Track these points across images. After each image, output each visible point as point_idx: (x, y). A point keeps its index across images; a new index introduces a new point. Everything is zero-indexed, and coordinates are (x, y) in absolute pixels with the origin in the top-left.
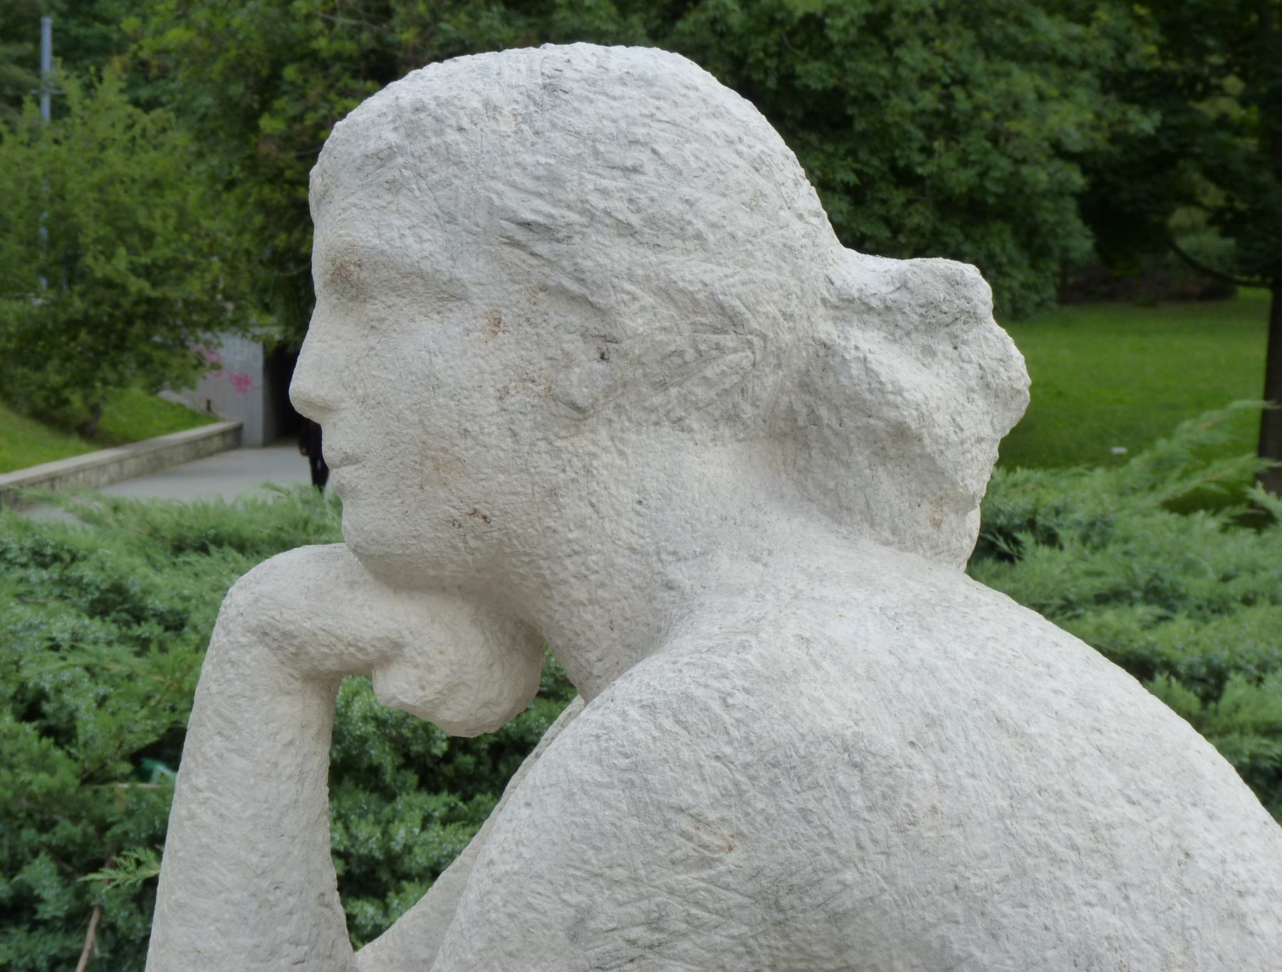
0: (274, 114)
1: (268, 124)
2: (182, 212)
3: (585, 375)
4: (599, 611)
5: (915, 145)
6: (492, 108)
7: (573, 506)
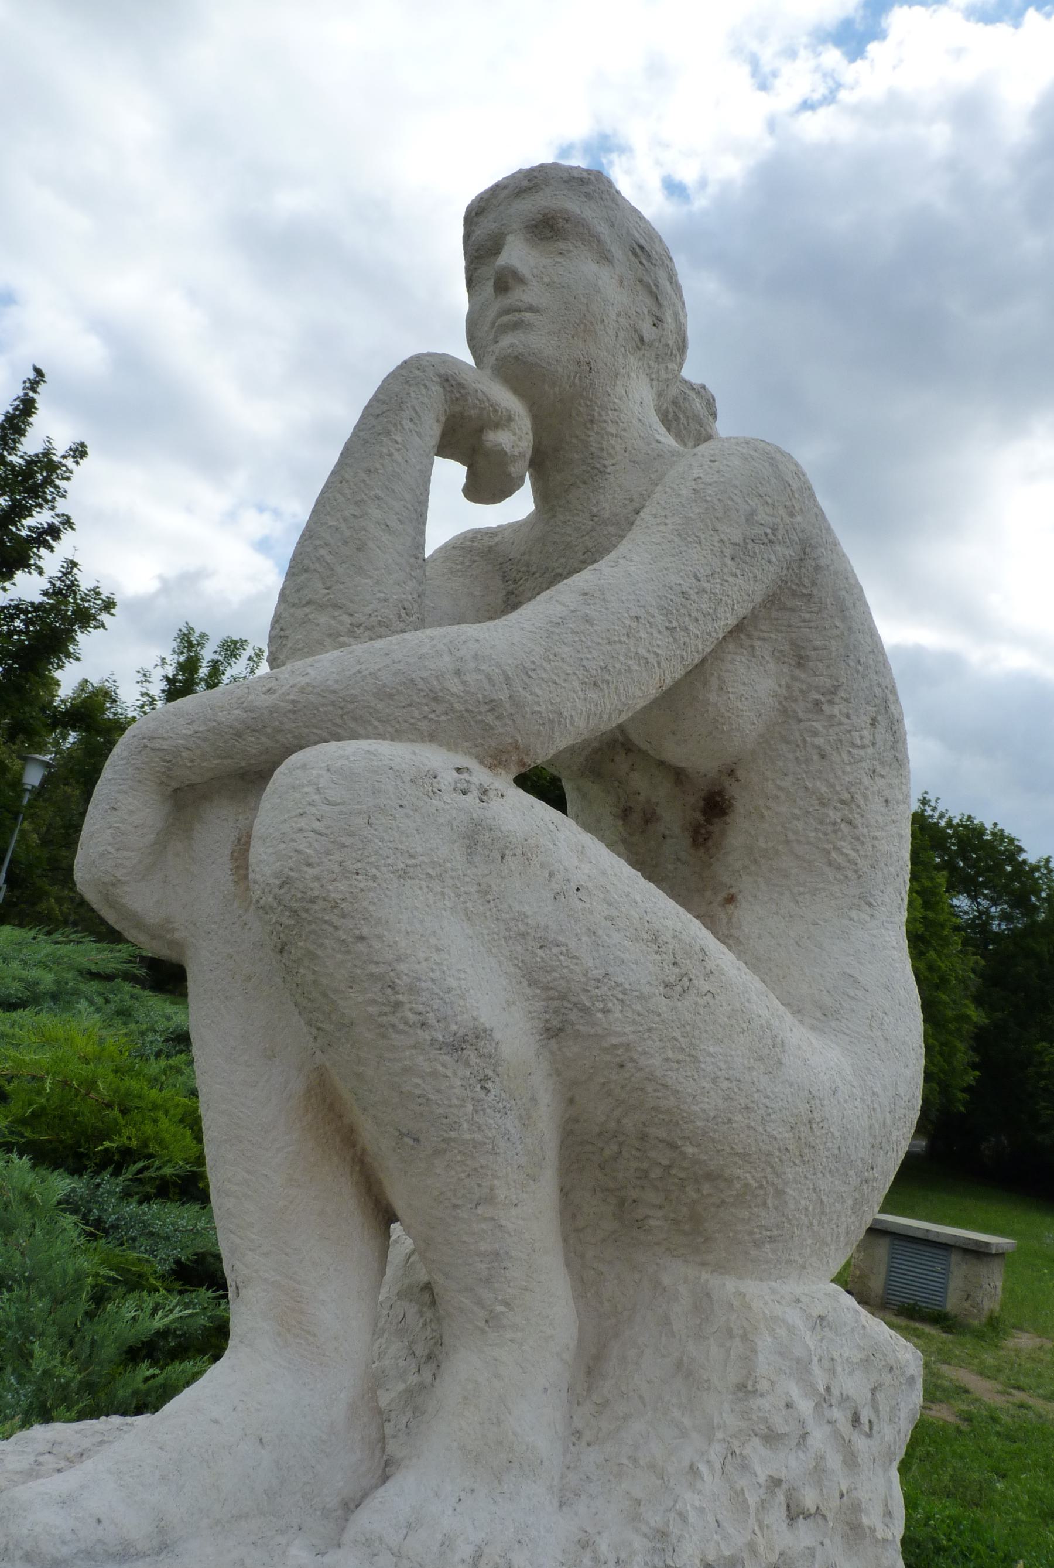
4: (619, 440)
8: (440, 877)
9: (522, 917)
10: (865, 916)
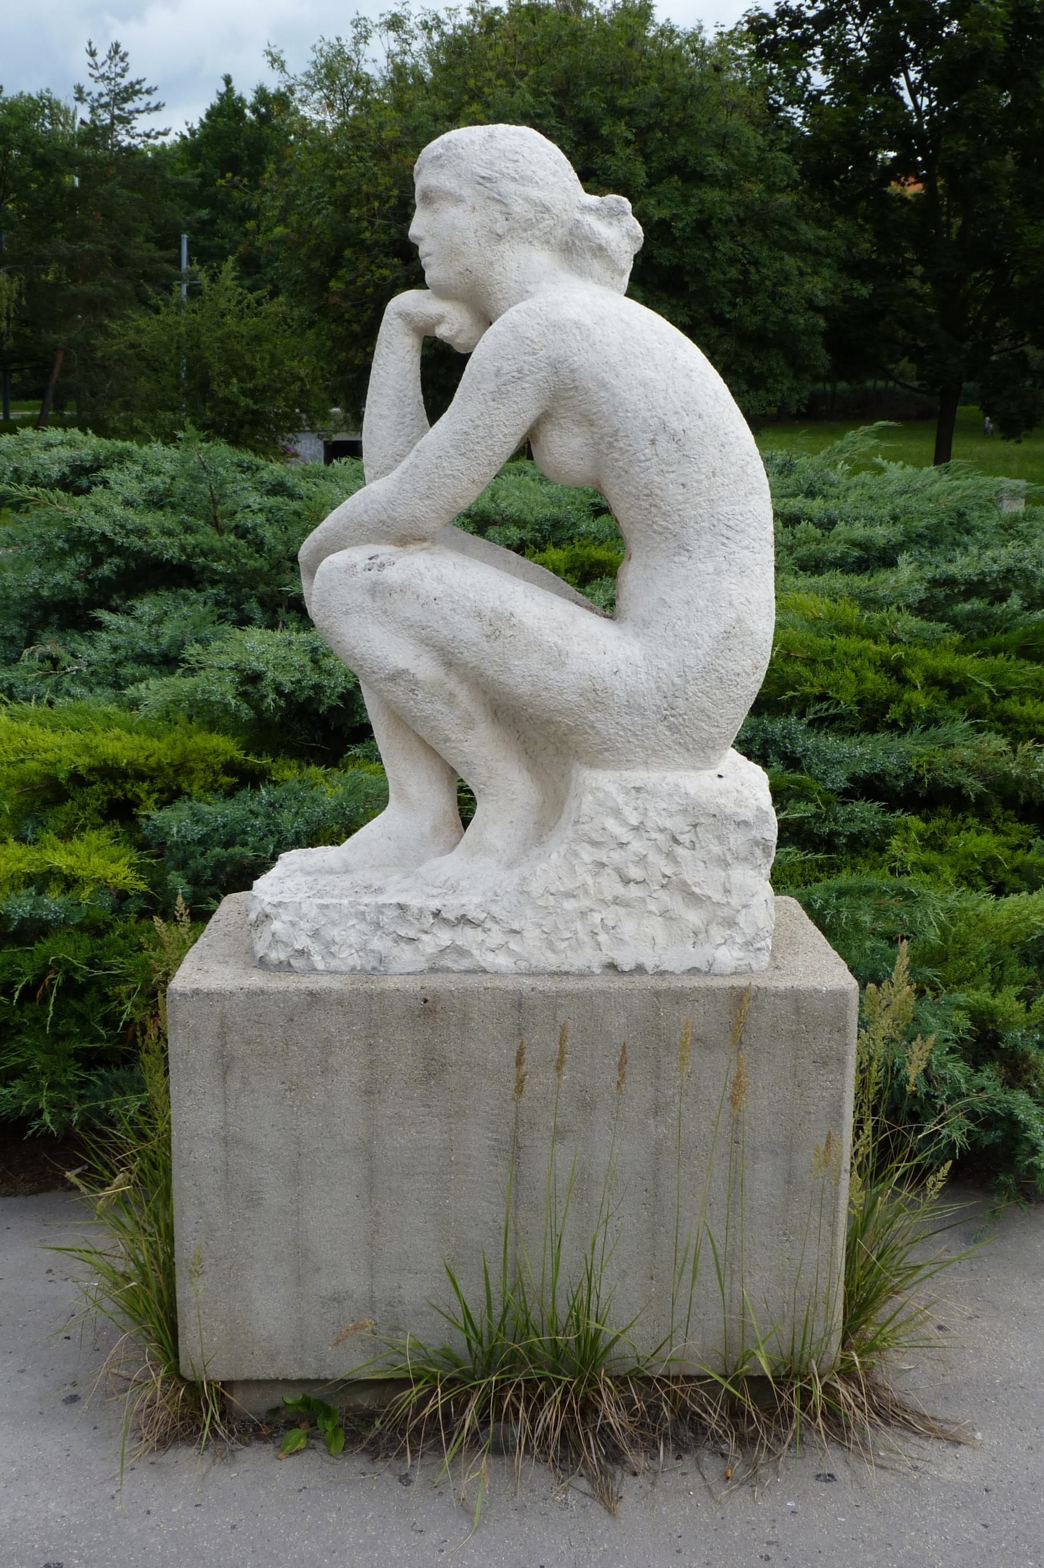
0: (338, 278)
1: (333, 284)
2: (273, 356)
3: (501, 226)
5: (726, 301)
6: (472, 142)
7: (498, 268)
8: (363, 610)
9: (407, 619)
10: (685, 559)
